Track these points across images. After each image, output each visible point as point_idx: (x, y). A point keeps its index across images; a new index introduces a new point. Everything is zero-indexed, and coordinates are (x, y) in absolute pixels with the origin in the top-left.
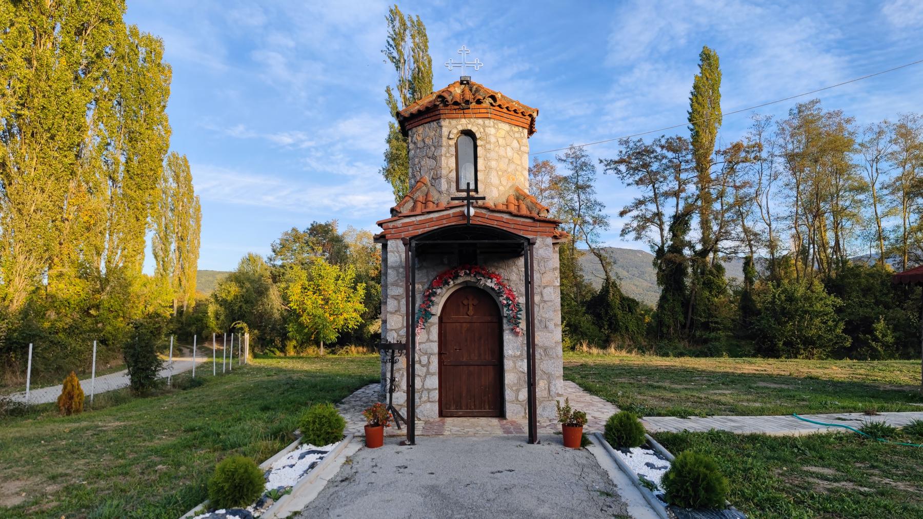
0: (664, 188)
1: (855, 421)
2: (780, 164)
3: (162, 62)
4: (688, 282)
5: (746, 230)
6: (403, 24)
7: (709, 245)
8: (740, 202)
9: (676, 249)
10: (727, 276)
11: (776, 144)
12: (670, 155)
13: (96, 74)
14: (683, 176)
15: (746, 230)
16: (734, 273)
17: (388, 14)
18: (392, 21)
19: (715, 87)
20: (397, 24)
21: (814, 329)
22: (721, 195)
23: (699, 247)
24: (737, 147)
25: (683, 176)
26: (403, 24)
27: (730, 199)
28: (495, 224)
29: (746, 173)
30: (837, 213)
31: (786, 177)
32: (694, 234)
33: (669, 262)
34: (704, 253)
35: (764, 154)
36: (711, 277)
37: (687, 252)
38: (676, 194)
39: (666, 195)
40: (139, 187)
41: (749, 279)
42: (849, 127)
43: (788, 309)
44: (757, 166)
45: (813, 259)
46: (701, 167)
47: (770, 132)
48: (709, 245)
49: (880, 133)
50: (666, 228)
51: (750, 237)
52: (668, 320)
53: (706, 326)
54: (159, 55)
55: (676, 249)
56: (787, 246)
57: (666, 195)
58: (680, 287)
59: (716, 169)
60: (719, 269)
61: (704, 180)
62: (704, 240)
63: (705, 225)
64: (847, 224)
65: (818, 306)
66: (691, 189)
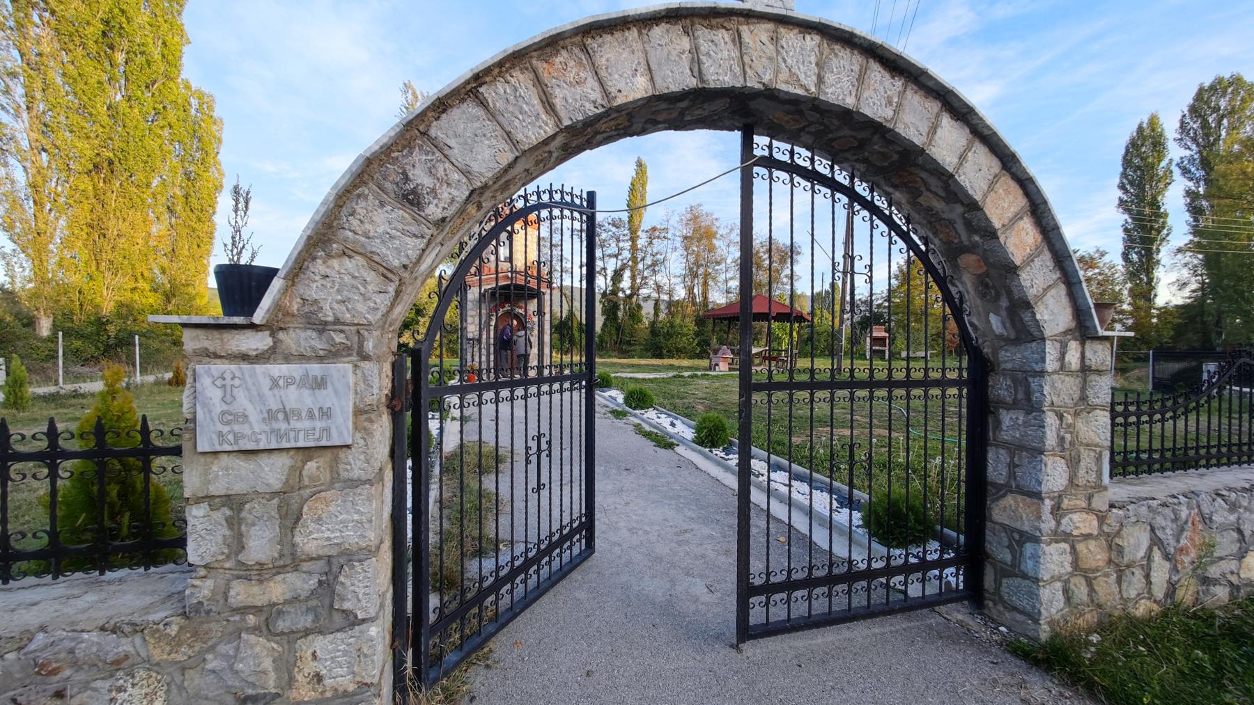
0: (609, 251)
1: (671, 374)
2: (678, 242)
3: (215, 114)
4: (620, 314)
5: (656, 283)
6: (414, 94)
7: (635, 289)
8: (654, 264)
9: (614, 293)
10: (643, 312)
11: (678, 229)
12: (614, 229)
13: (162, 123)
14: (621, 244)
15: (656, 283)
16: (647, 309)
17: (402, 86)
18: (406, 92)
19: (644, 185)
20: (410, 96)
21: (683, 342)
22: (643, 259)
23: (628, 292)
24: (654, 229)
25: (621, 244)
26: (414, 94)
27: (649, 261)
28: (428, 454)
29: (658, 245)
30: (707, 275)
31: (681, 251)
32: (626, 283)
33: (610, 301)
34: (630, 297)
35: (669, 236)
36: (634, 314)
37: (621, 294)
38: (616, 256)
39: (610, 256)
40: (200, 220)
41: (656, 314)
42: (717, 224)
43: (671, 332)
44: (666, 242)
45: (1240, 413)
46: (633, 239)
47: (674, 220)
48: (635, 289)
49: (732, 230)
50: (609, 278)
51: (659, 288)
52: (607, 339)
53: (629, 343)
54: (210, 108)
55: (614, 293)
56: (681, 294)
57: (610, 256)
58: (615, 317)
59: (641, 242)
60: (639, 307)
61: (634, 248)
62: (632, 287)
63: (633, 278)
64: (710, 282)
65: (685, 330)
66: (627, 254)
